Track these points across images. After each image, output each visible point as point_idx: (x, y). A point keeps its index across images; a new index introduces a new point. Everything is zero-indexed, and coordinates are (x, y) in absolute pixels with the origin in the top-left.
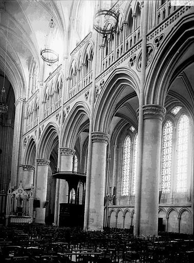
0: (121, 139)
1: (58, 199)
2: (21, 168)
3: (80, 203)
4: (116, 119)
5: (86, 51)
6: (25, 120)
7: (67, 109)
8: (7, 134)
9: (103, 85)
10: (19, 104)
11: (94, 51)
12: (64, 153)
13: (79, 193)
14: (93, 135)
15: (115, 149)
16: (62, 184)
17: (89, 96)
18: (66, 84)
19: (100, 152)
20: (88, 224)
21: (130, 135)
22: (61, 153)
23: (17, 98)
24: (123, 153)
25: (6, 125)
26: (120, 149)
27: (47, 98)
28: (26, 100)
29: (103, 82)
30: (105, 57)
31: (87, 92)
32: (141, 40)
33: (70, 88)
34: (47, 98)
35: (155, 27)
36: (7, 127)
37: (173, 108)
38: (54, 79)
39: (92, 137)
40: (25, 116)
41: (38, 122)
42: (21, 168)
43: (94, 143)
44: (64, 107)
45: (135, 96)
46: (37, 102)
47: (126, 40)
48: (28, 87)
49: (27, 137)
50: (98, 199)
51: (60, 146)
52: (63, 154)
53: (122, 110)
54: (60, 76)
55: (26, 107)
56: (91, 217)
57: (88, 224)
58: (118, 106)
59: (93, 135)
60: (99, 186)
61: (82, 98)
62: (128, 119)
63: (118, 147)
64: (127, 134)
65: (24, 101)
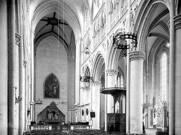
0: (158, 56)
1: (107, 110)
2: (82, 90)
3: (124, 112)
4: (152, 40)
5: (102, 16)
6: (82, 54)
7: (110, 38)
8: (72, 66)
9: (137, 10)
10: (78, 42)
11: (106, 16)
12: (110, 73)
13: (122, 103)
14: (130, 54)
15: (153, 65)
16: (110, 98)
17: (126, 23)
18: (108, 18)
19: (138, 69)
20: (129, 129)
21: (166, 51)
22: (107, 74)
23: (76, 38)
24: (160, 68)
25: (71, 60)
26: (157, 64)
27: (96, 33)
28: (82, 39)
29: (137, 7)
30: (112, 20)
31: (124, 19)
32: (127, 10)
33: (111, 20)
34: (96, 33)
35: (117, 23)
36: (72, 61)
37: (161, 54)
38: (100, 16)
39: (130, 56)
40: (82, 51)
41: (106, 34)
42: (82, 90)
43: (131, 62)
44: (107, 37)
45: (168, 13)
46: (89, 38)
47: (102, 35)
48: (83, 29)
49: (84, 66)
50: (137, 109)
51: (106, 69)
52: (109, 74)
53: (156, 30)
54: (104, 13)
55: (83, 43)
56: (131, 123)
57: (129, 129)
58: (151, 27)
59: (130, 54)
60: (137, 97)
61: (120, 26)
62: (163, 37)
63: (155, 63)
64: (164, 50)
65: (82, 39)
